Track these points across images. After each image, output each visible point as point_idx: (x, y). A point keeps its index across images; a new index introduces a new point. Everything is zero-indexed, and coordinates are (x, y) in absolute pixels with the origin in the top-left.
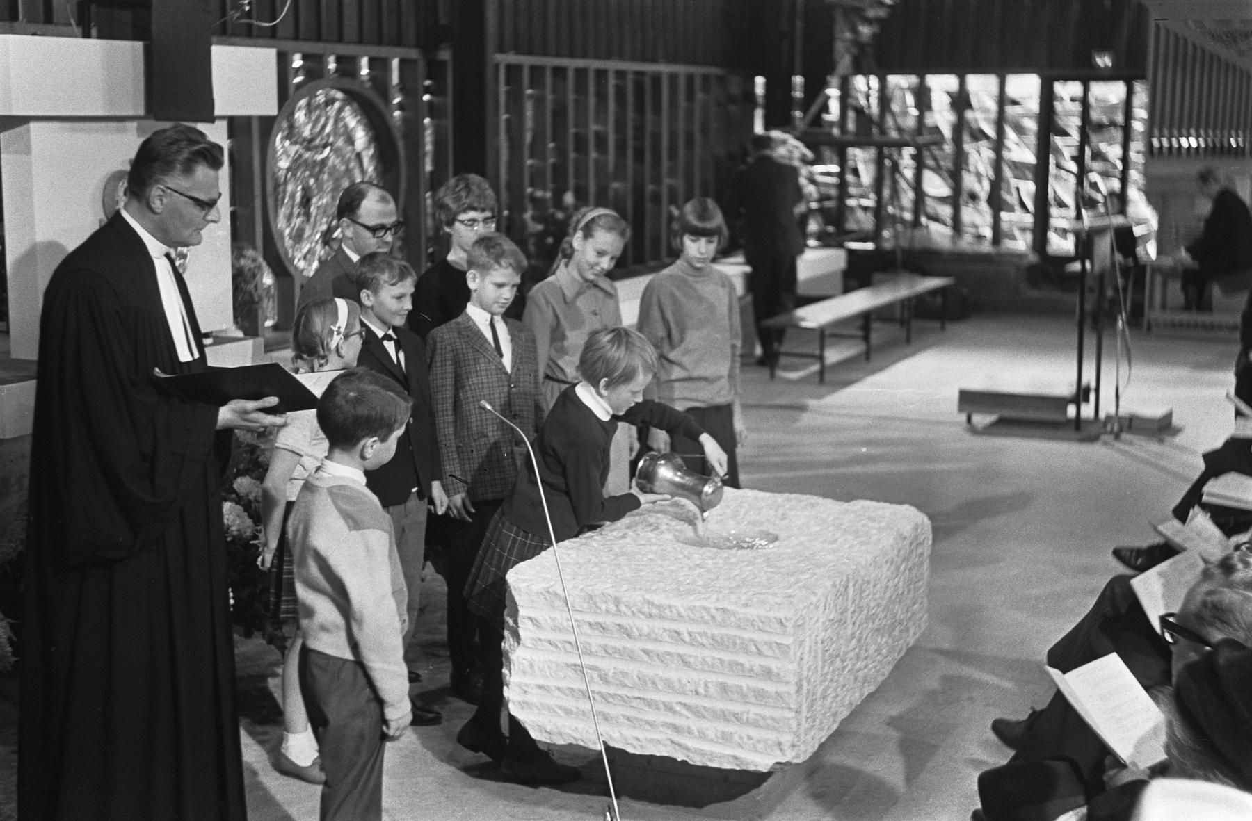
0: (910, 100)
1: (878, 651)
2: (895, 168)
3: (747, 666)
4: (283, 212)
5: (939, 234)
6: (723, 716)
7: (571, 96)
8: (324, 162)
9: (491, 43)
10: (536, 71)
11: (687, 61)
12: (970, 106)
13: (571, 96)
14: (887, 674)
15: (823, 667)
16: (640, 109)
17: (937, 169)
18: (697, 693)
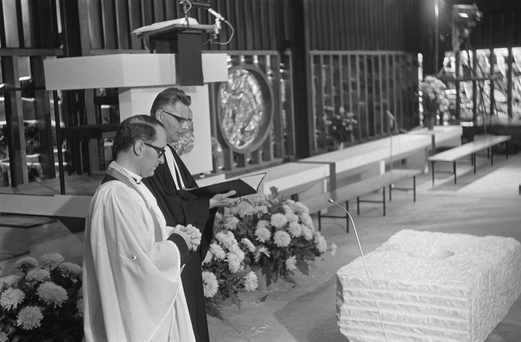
0: (487, 60)
1: (503, 303)
2: (482, 90)
3: (447, 311)
4: (225, 121)
5: (502, 117)
6: (436, 333)
7: (341, 67)
8: (240, 100)
9: (308, 47)
10: (326, 57)
11: (389, 49)
12: (514, 61)
13: (341, 67)
14: (506, 313)
15: (480, 311)
16: (370, 71)
17: (500, 89)
18: (424, 323)
